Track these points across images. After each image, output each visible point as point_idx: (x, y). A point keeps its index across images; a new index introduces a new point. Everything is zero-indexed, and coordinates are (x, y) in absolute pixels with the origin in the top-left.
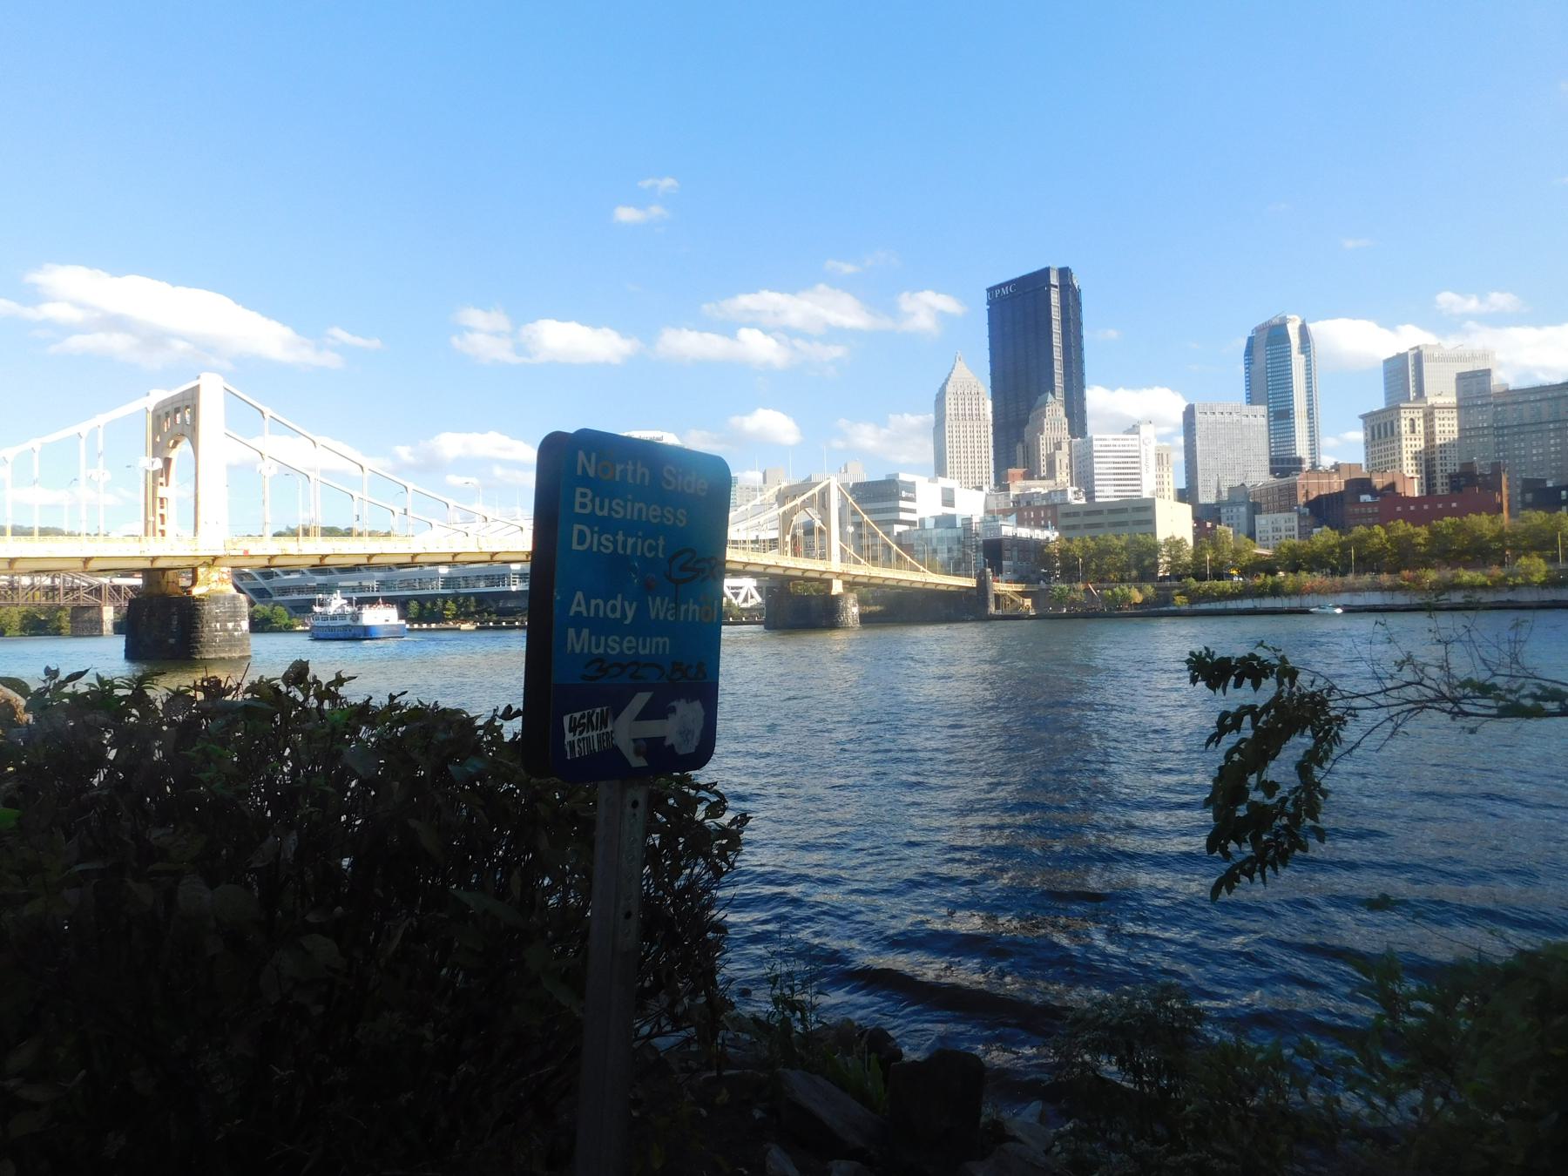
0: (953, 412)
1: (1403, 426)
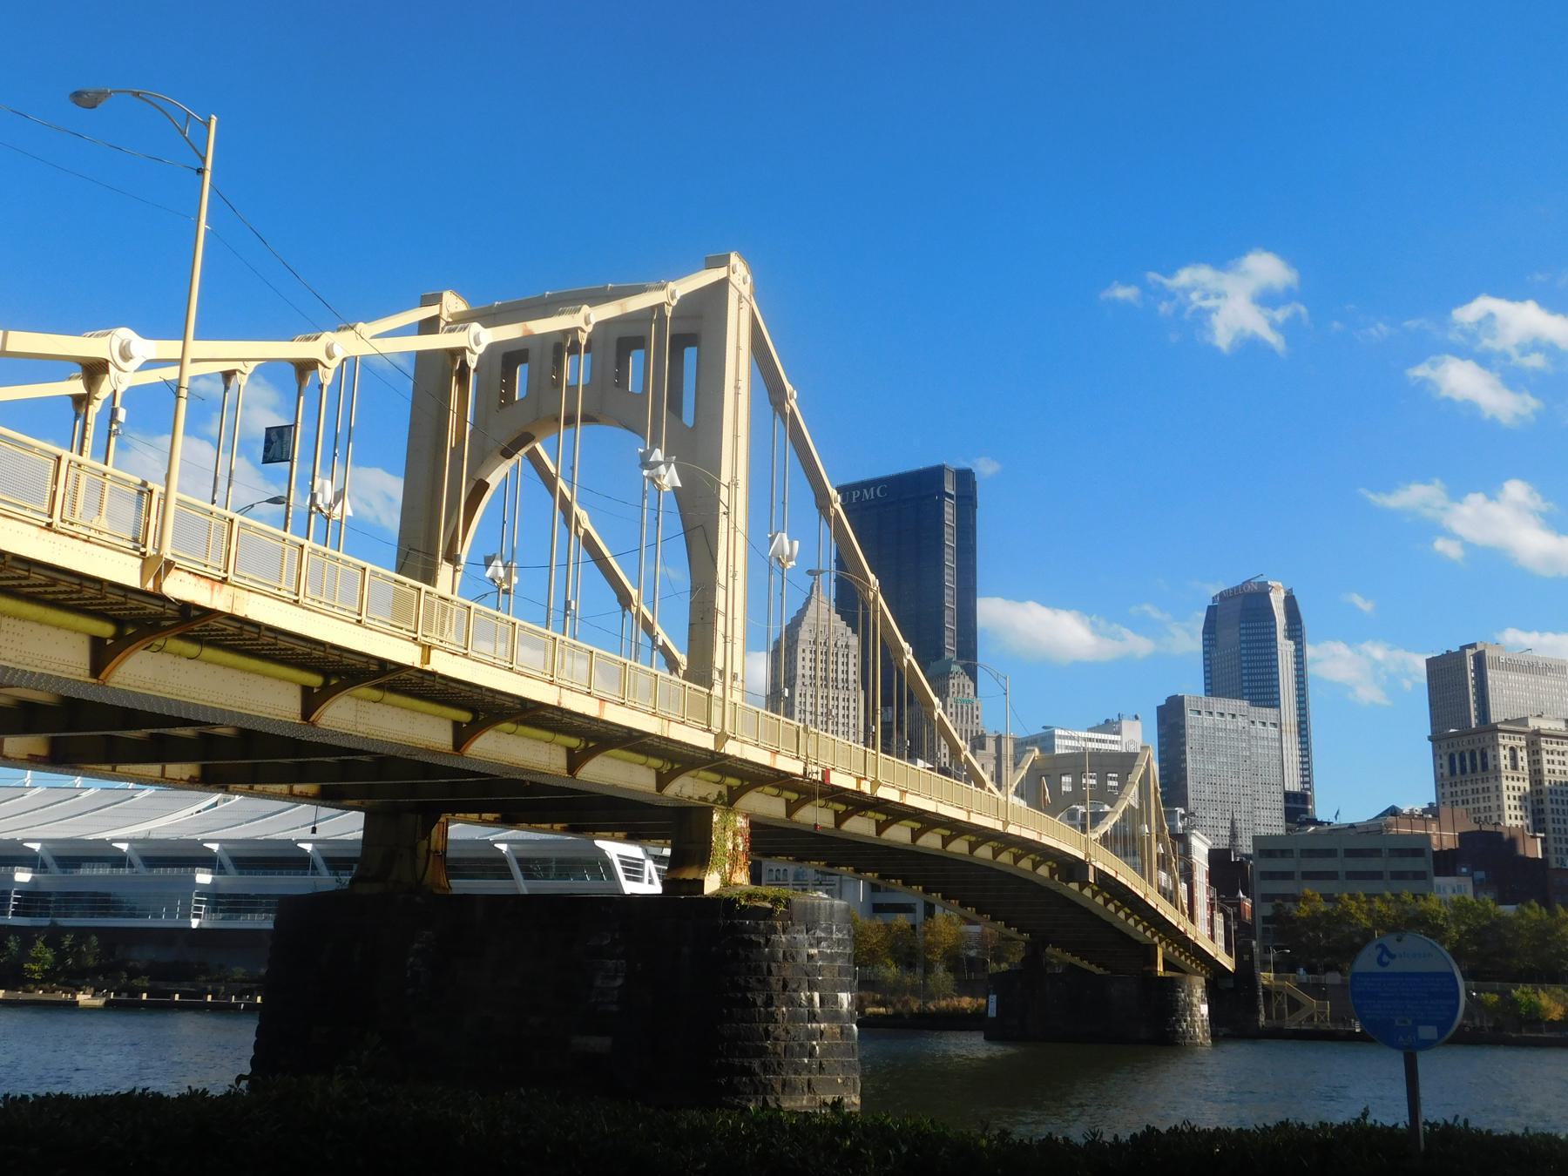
0: (808, 673)
1: (1502, 758)
